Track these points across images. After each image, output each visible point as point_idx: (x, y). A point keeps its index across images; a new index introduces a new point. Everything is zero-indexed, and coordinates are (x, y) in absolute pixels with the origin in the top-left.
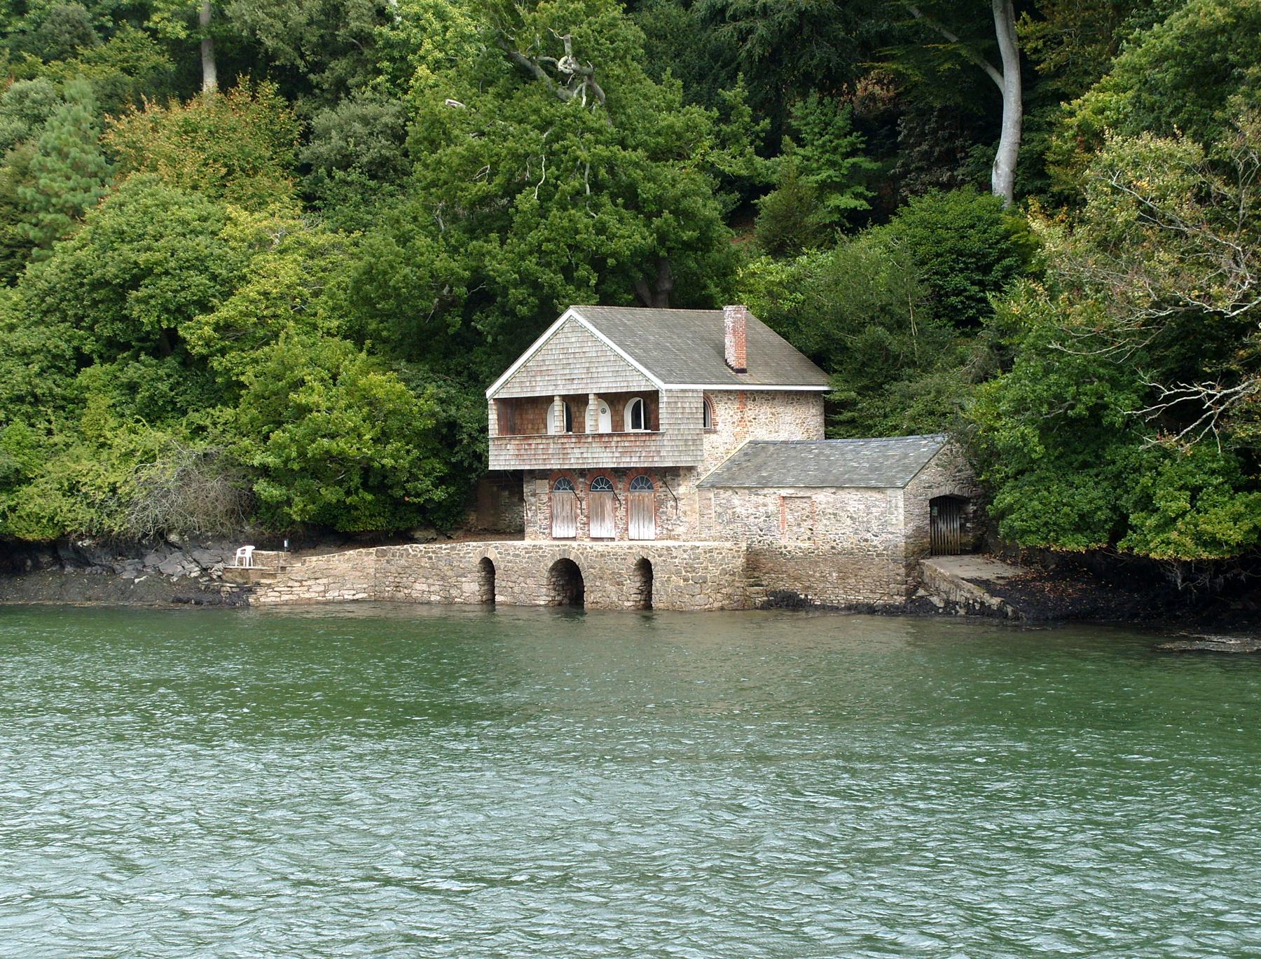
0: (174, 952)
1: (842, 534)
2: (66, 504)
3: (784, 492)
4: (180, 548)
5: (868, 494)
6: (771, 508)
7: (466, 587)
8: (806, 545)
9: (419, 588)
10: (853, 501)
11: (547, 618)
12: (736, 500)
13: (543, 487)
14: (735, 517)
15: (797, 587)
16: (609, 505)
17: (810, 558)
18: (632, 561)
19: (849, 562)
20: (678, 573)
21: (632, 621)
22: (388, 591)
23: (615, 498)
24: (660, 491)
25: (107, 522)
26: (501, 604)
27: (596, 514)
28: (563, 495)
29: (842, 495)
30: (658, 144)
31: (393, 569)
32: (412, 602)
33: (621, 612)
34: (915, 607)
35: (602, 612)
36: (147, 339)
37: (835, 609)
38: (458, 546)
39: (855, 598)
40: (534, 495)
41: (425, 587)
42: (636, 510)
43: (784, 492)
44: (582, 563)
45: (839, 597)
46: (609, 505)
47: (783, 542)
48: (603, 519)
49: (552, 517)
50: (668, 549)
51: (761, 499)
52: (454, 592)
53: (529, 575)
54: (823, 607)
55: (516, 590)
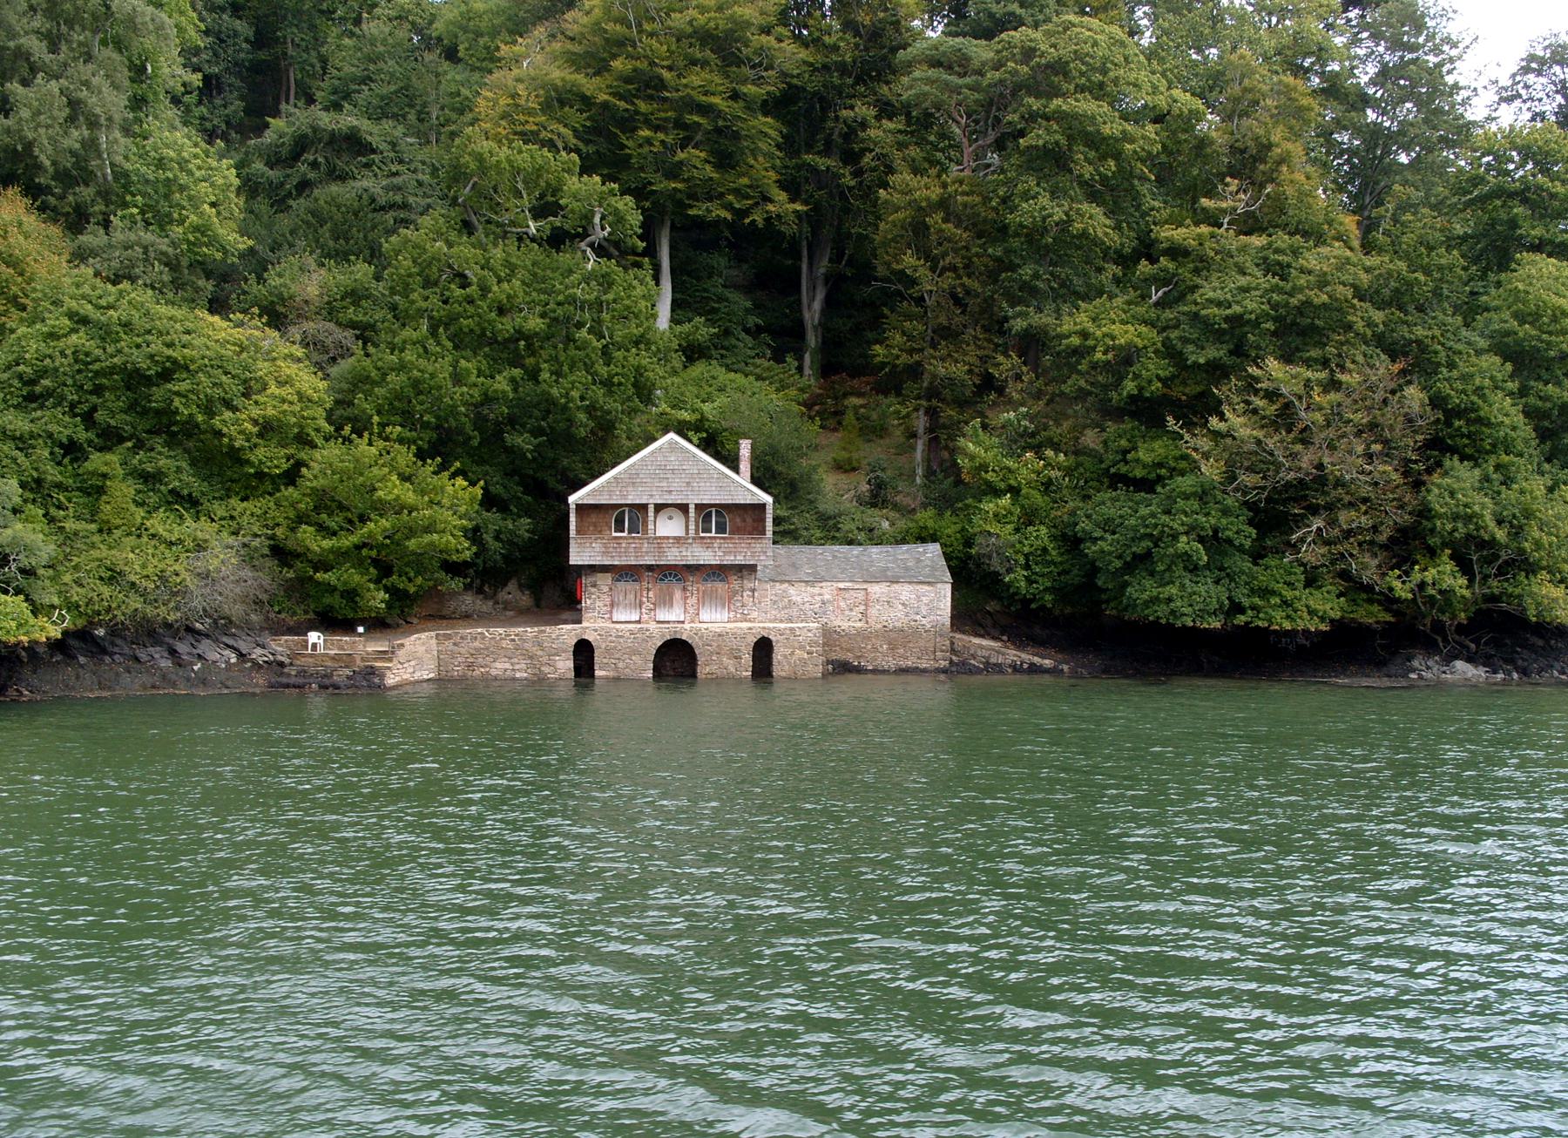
0: (160, 1119)
1: (896, 617)
2: (106, 591)
3: (841, 585)
4: (207, 636)
5: (919, 587)
6: (827, 597)
7: (560, 665)
8: (859, 625)
9: (500, 667)
10: (906, 592)
11: (650, 690)
12: (792, 591)
13: (604, 580)
14: (791, 604)
15: (849, 657)
16: (678, 594)
17: (864, 635)
18: (752, 640)
19: (897, 637)
20: (802, 648)
21: (749, 692)
22: (458, 671)
23: (684, 589)
24: (735, 584)
25: (149, 609)
26: (601, 678)
27: (666, 601)
28: (630, 586)
29: (896, 587)
30: (1303, 195)
31: (463, 651)
32: (487, 679)
33: (740, 680)
34: (958, 668)
35: (717, 681)
36: (134, 420)
37: (884, 672)
38: (548, 629)
39: (903, 664)
40: (594, 586)
41: (507, 666)
42: (706, 599)
43: (841, 585)
44: (695, 642)
45: (891, 663)
46: (678, 594)
47: (837, 623)
48: (671, 606)
49: (612, 605)
50: (792, 629)
51: (816, 590)
52: (546, 669)
53: (635, 652)
54: (875, 671)
55: (621, 665)
